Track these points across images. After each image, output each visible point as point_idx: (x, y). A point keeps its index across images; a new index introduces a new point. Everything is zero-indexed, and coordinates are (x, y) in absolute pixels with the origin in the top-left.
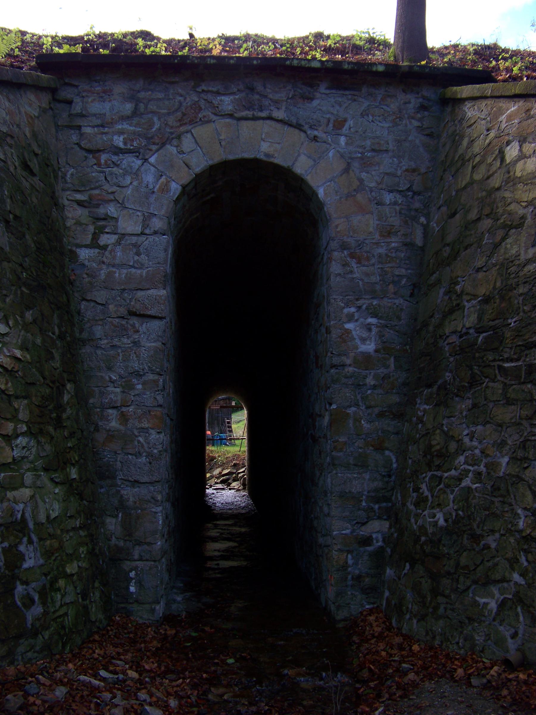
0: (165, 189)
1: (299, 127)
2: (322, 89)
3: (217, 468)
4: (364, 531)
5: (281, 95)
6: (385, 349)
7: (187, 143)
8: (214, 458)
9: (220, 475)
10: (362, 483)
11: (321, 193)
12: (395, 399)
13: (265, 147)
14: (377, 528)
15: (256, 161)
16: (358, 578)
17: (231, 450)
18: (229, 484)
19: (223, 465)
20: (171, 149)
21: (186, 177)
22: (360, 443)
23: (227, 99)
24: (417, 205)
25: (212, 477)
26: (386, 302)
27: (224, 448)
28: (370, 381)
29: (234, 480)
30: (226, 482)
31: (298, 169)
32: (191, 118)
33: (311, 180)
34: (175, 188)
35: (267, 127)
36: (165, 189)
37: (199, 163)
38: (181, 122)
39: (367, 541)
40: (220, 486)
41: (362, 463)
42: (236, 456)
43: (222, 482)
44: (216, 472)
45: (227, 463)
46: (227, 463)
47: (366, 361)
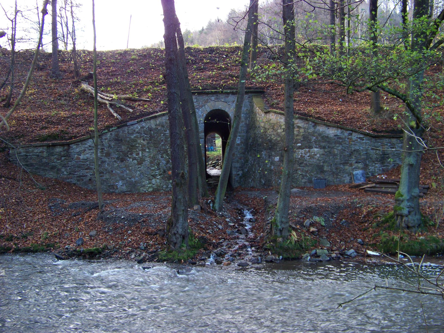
0: (203, 115)
1: (226, 102)
2: (230, 95)
3: (367, 253)
4: (238, 173)
5: (223, 97)
6: (241, 142)
7: (206, 106)
8: (209, 157)
9: (212, 163)
10: (238, 165)
11: (230, 115)
12: (243, 151)
13: (220, 106)
14: (240, 173)
15: (219, 109)
16: (237, 181)
17: (215, 154)
18: (215, 167)
19: (213, 160)
20: (203, 107)
21: (207, 113)
22: (237, 159)
23: (213, 98)
24: (248, 116)
25: (208, 164)
26: (242, 134)
27: (213, 153)
28: (239, 148)
29: (217, 166)
30: (214, 167)
31: (226, 111)
32: (207, 102)
33: (229, 113)
34: (205, 115)
35: (220, 103)
36: (203, 115)
37: (209, 110)
38: (205, 102)
39: (239, 175)
40: (212, 168)
41: (238, 162)
42: (218, 156)
43: (212, 166)
44: (210, 162)
45: (214, 159)
46: (214, 159)
47: (238, 145)
